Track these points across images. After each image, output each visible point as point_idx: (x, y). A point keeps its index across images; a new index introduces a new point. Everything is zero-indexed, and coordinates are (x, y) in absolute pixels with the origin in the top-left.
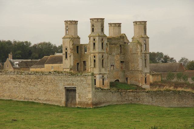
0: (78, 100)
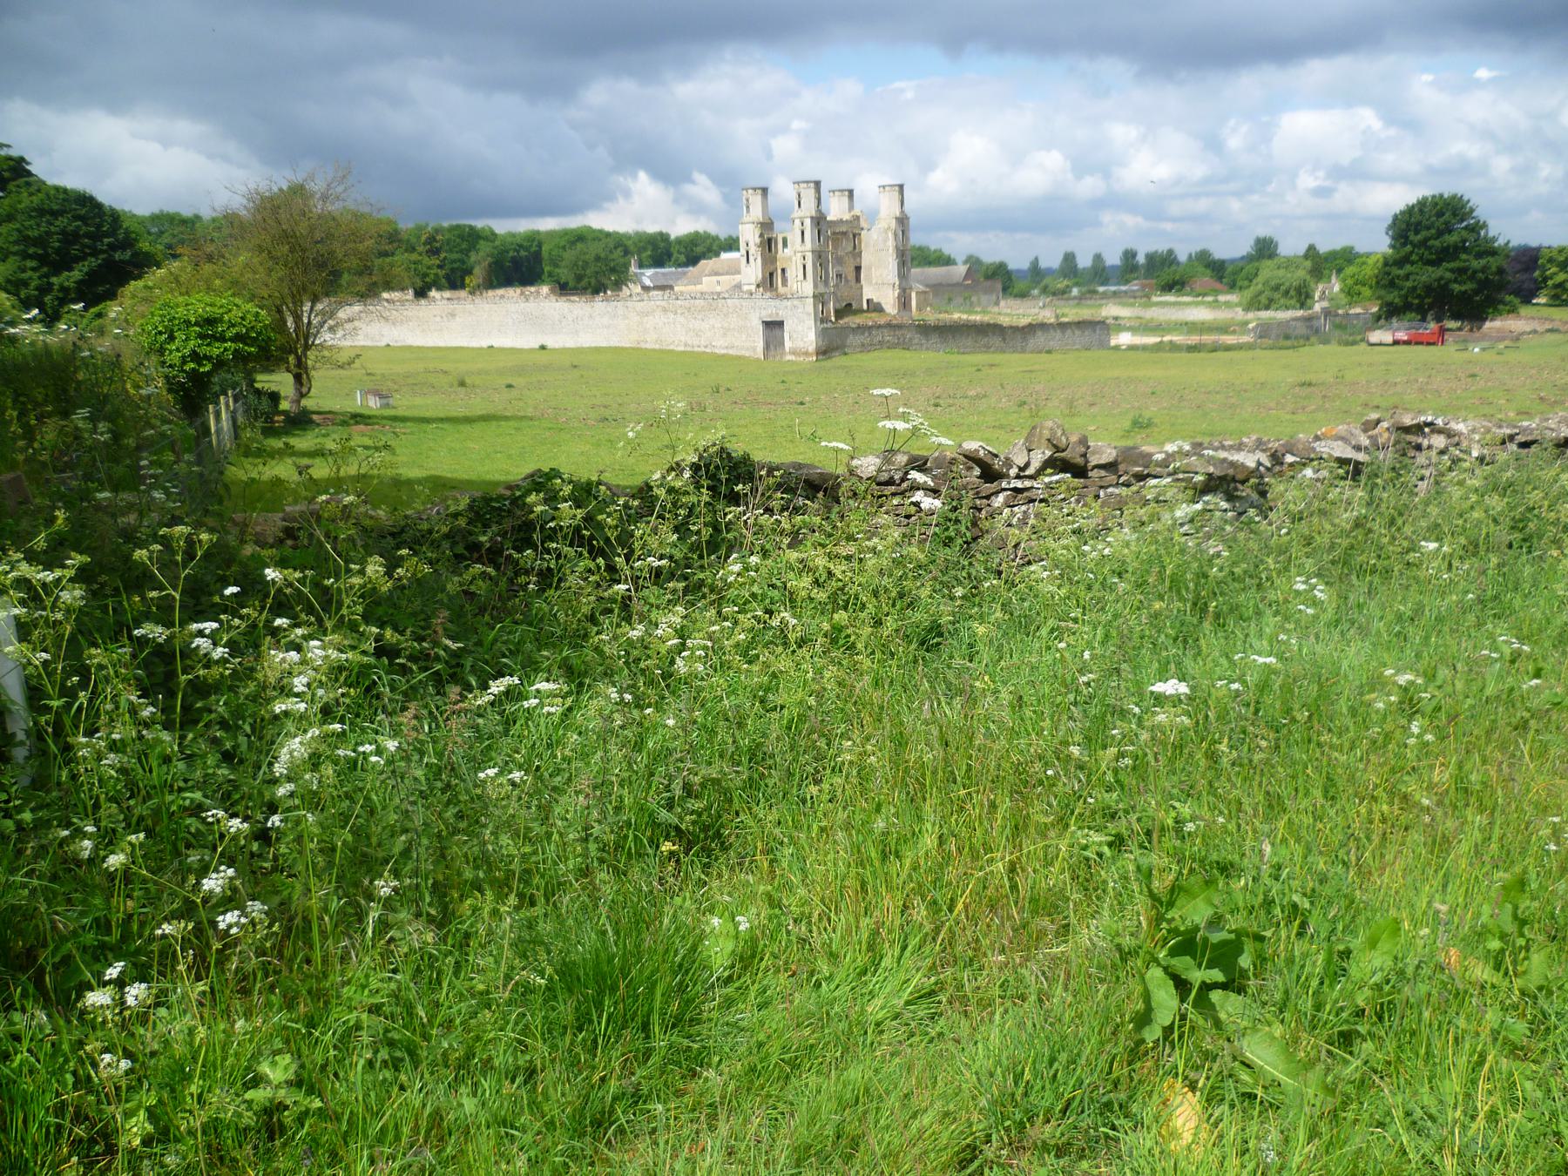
0: (788, 344)
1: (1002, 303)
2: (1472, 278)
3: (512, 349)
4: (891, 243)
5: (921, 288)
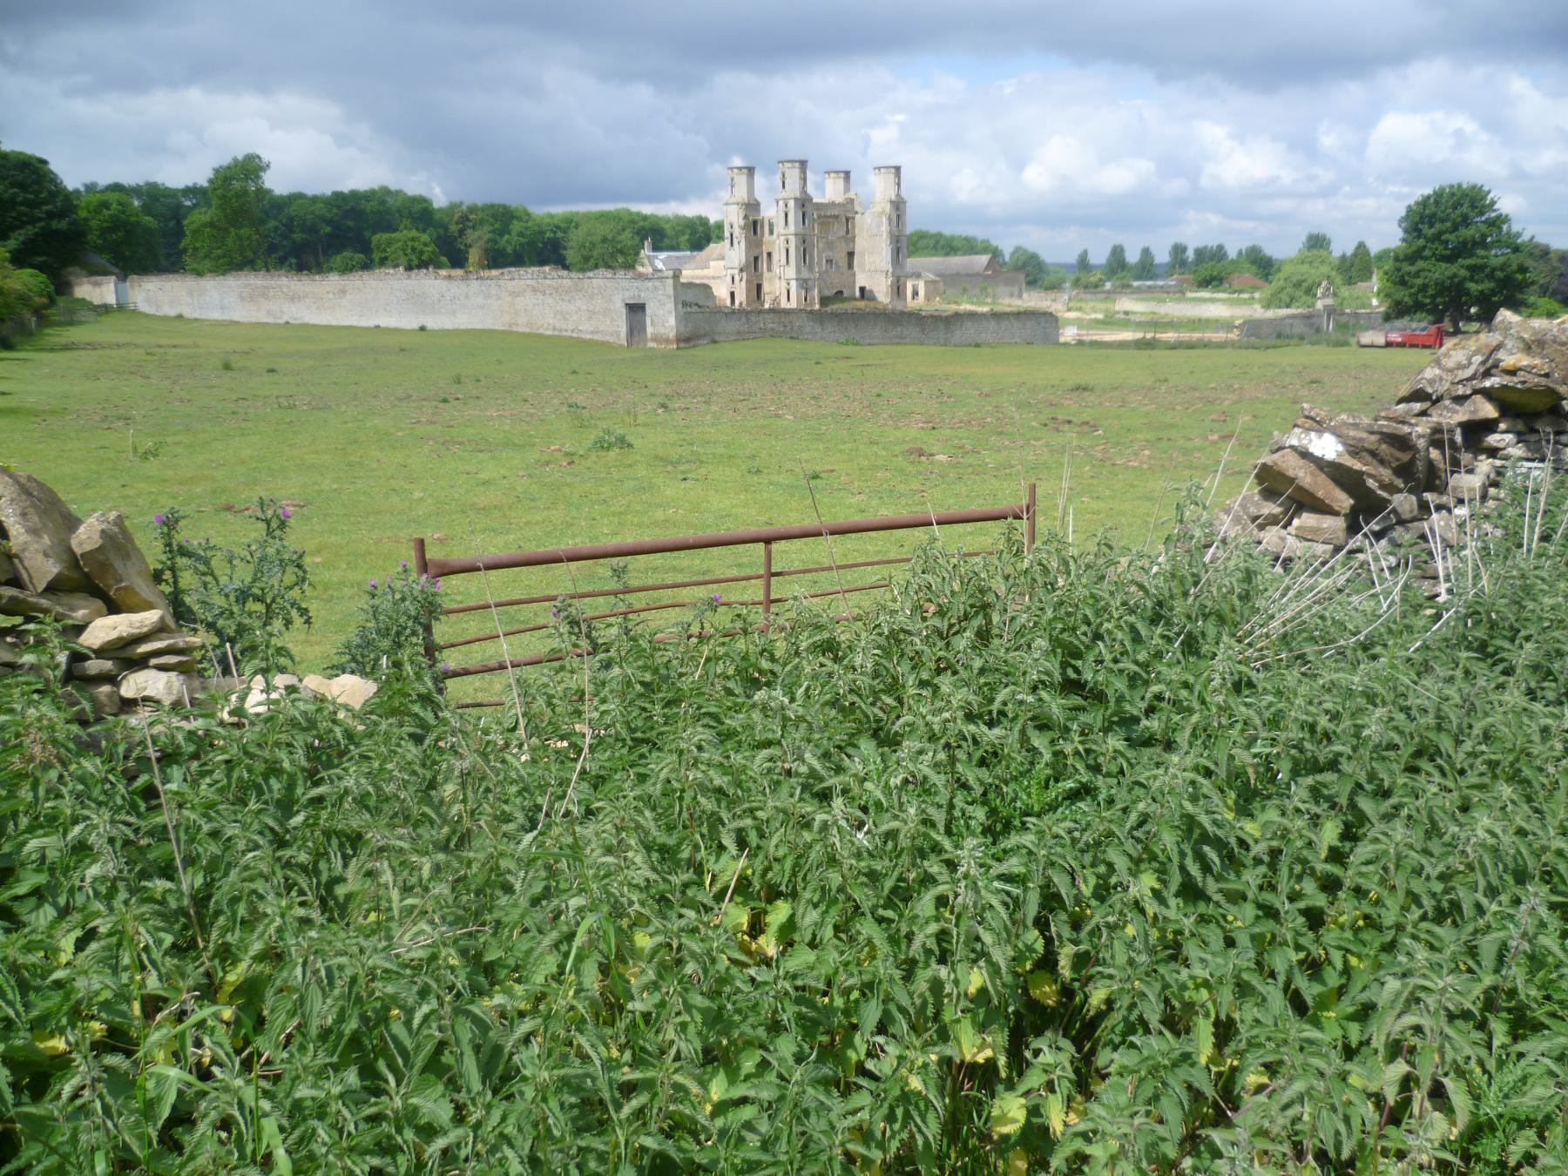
0: (650, 330)
1: (1025, 295)
2: (1491, 276)
3: (484, 331)
4: (885, 228)
5: (932, 277)
